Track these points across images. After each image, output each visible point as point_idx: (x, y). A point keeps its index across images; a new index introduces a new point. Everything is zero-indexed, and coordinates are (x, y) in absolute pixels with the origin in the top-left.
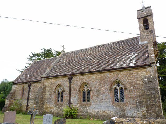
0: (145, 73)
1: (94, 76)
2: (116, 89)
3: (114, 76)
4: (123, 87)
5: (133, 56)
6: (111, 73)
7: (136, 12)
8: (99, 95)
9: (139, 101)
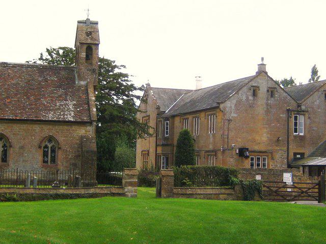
0: (84, 131)
1: (16, 127)
2: (46, 147)
3: (47, 131)
4: (56, 146)
5: (71, 104)
6: (43, 126)
7: (76, 24)
8: (23, 154)
9: (73, 164)
